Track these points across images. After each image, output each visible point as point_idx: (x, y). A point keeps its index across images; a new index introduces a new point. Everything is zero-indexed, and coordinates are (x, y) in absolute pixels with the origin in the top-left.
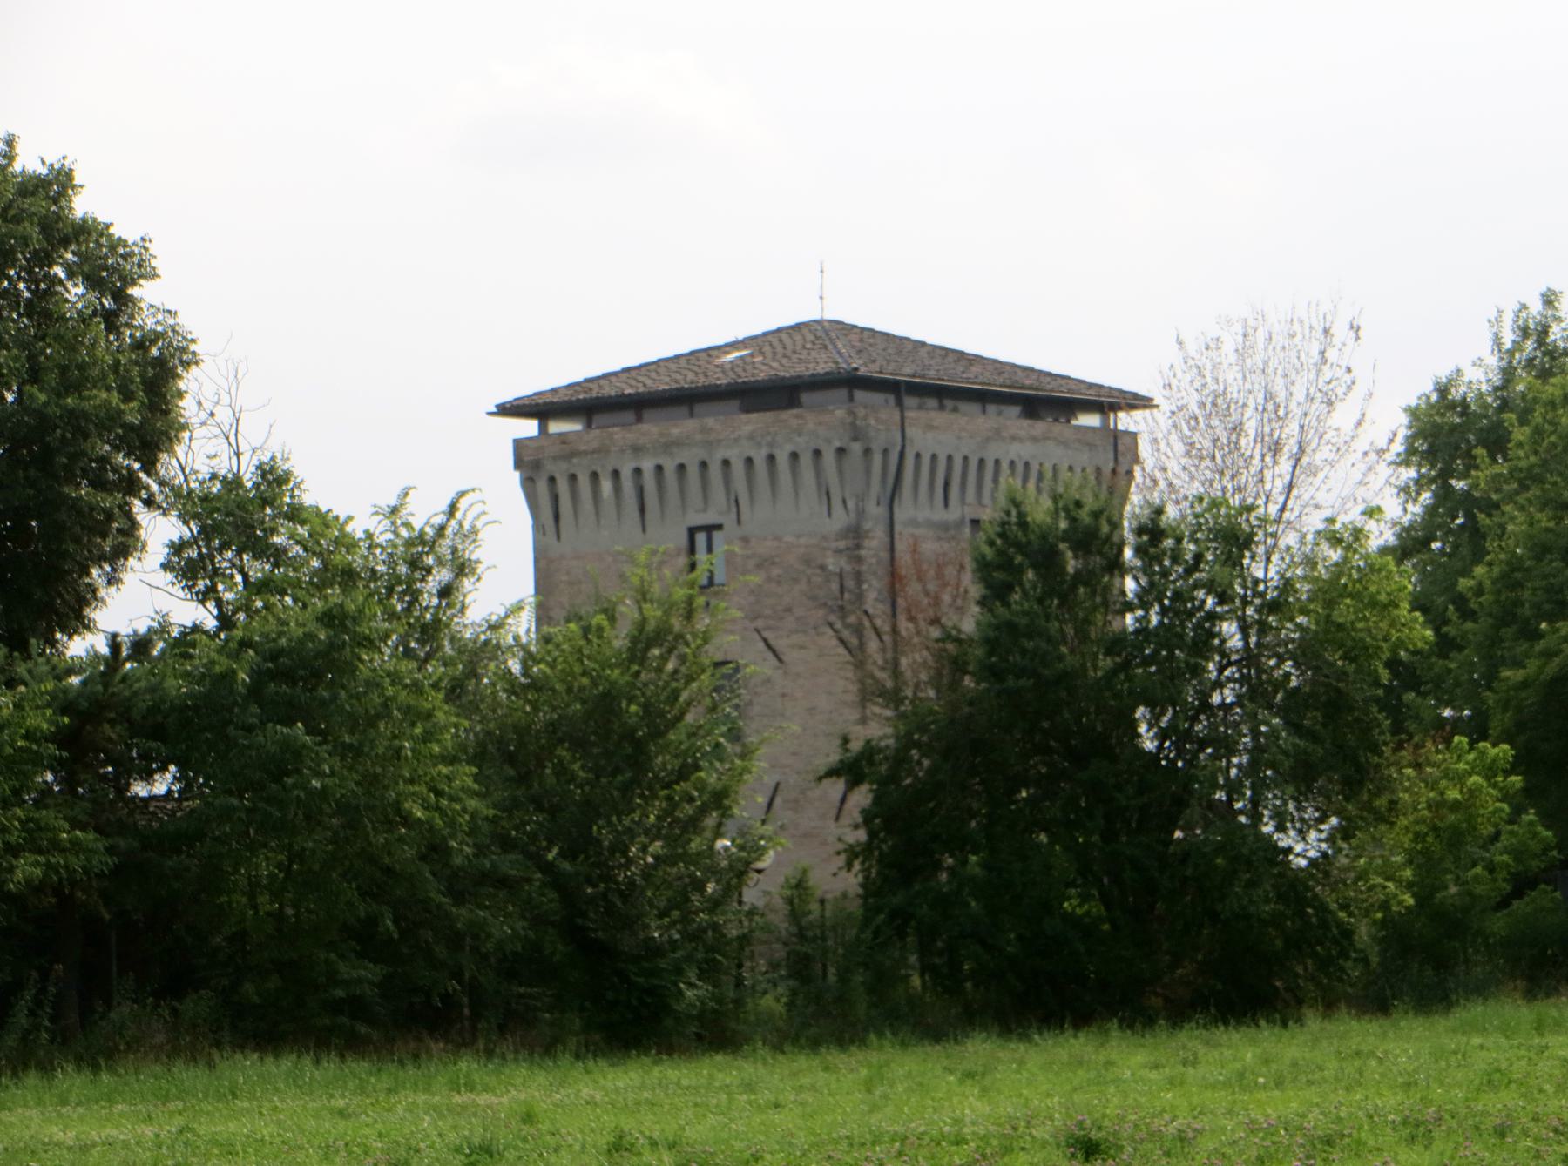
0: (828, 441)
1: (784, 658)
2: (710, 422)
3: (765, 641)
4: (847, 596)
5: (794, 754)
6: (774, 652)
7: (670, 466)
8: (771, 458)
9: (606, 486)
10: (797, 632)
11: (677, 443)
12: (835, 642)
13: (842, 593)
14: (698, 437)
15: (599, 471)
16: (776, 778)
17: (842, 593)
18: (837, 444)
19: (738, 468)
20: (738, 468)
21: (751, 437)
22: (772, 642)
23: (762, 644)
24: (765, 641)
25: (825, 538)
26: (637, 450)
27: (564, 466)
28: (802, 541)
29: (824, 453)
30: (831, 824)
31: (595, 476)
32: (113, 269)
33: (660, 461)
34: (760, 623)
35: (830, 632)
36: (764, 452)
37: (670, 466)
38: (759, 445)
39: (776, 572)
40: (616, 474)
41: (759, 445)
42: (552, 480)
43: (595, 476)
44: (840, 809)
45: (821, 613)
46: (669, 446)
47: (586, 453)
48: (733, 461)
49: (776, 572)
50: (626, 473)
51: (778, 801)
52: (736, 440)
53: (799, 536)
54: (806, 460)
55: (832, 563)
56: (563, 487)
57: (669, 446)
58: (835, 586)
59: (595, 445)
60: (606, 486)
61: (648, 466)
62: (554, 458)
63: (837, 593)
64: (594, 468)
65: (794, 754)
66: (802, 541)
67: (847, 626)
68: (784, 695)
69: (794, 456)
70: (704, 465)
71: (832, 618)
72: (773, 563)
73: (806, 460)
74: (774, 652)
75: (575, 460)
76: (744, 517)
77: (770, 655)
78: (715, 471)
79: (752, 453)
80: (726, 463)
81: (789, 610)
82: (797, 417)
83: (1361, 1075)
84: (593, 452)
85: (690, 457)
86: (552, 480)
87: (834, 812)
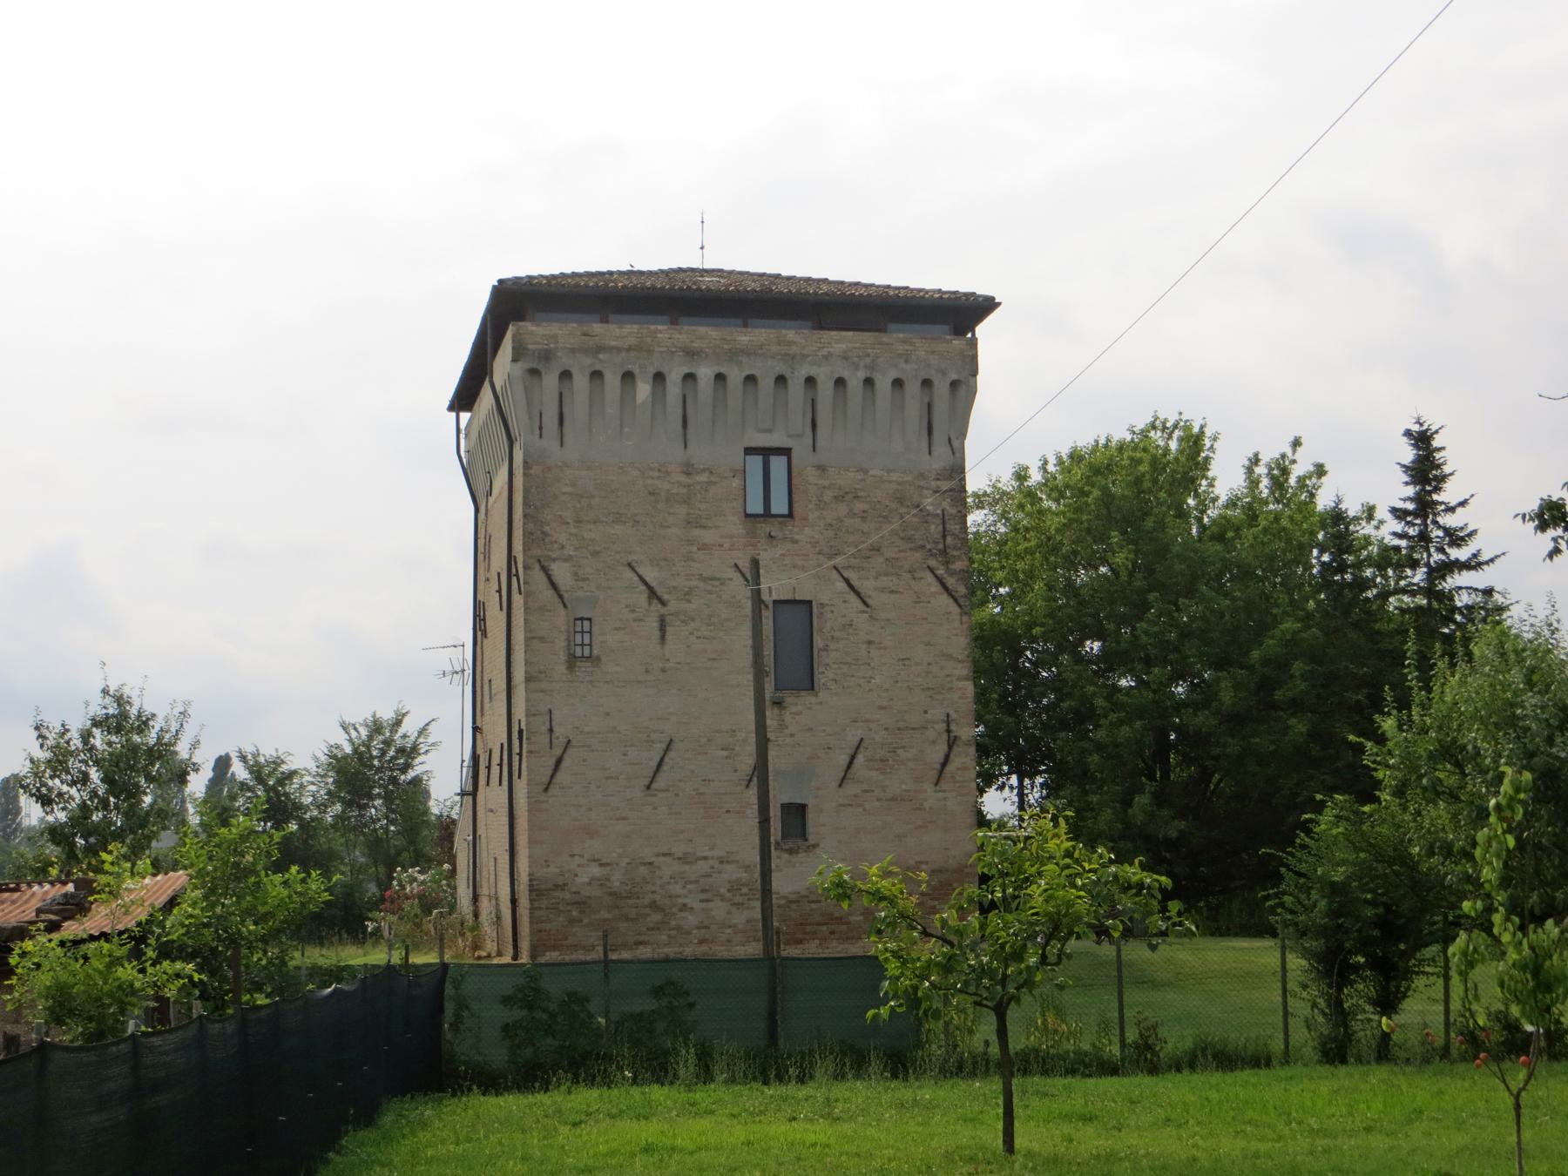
0: (944, 373)
1: (869, 601)
2: (791, 334)
3: (847, 581)
4: (949, 540)
5: (881, 708)
6: (858, 594)
7: (735, 376)
8: (869, 382)
9: (643, 389)
10: (887, 575)
11: (748, 352)
12: (936, 587)
13: (944, 537)
14: (774, 348)
15: (636, 371)
16: (859, 733)
17: (944, 537)
18: (954, 377)
19: (826, 388)
20: (826, 388)
21: (845, 357)
22: (855, 583)
23: (841, 585)
24: (847, 581)
25: (922, 476)
26: (691, 354)
27: (587, 361)
28: (895, 476)
29: (936, 383)
30: (929, 788)
31: (628, 377)
32: (973, 294)
33: (723, 370)
34: (838, 560)
35: (930, 578)
36: (862, 374)
37: (735, 376)
38: (856, 367)
39: (859, 506)
40: (659, 377)
41: (856, 367)
42: (566, 375)
43: (628, 377)
44: (941, 772)
45: (918, 555)
46: (735, 355)
47: (619, 350)
48: (821, 380)
49: (859, 506)
50: (674, 376)
51: (860, 759)
52: (827, 357)
53: (889, 471)
54: (913, 388)
55: (929, 502)
56: (581, 381)
57: (735, 355)
58: (934, 529)
59: (632, 341)
60: (643, 389)
61: (705, 372)
62: (573, 351)
63: (938, 536)
64: (630, 367)
65: (881, 708)
66: (895, 476)
67: (952, 573)
68: (870, 643)
69: (898, 383)
70: (781, 380)
71: (932, 563)
72: (856, 497)
73: (913, 388)
74: (858, 594)
75: (601, 356)
76: (819, 444)
77: (852, 597)
78: (796, 386)
79: (845, 374)
80: (810, 381)
81: (876, 549)
82: (904, 341)
83: (1130, 887)
84: (629, 349)
85: (765, 372)
86: (566, 375)
87: (934, 774)
